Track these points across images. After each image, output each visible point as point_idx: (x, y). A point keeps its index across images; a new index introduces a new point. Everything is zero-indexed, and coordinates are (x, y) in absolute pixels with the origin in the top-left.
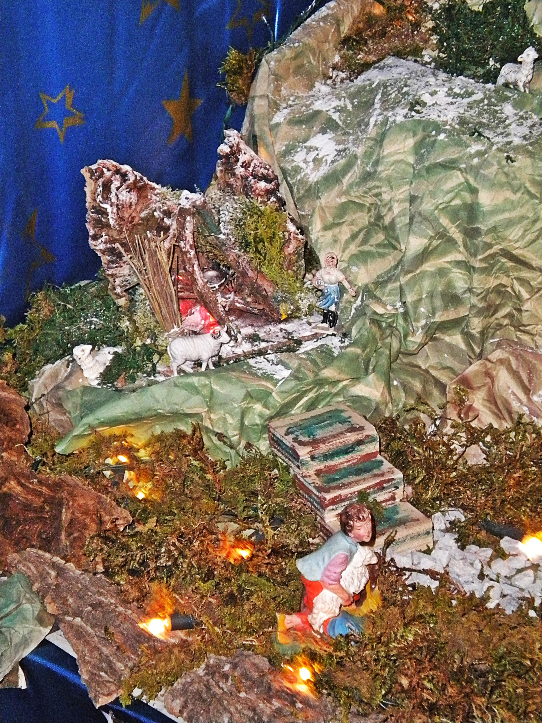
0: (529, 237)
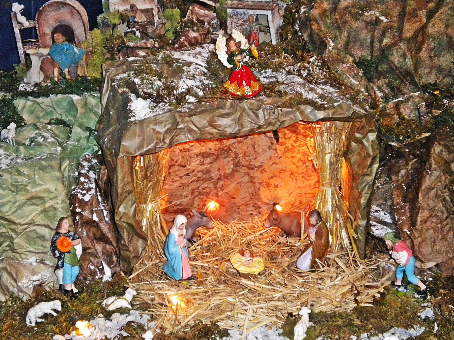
0: (13, 210)
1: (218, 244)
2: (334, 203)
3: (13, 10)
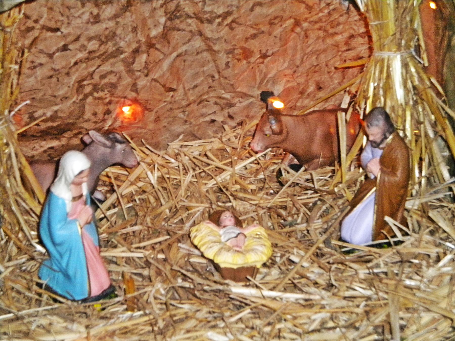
1: (152, 200)
2: (410, 85)
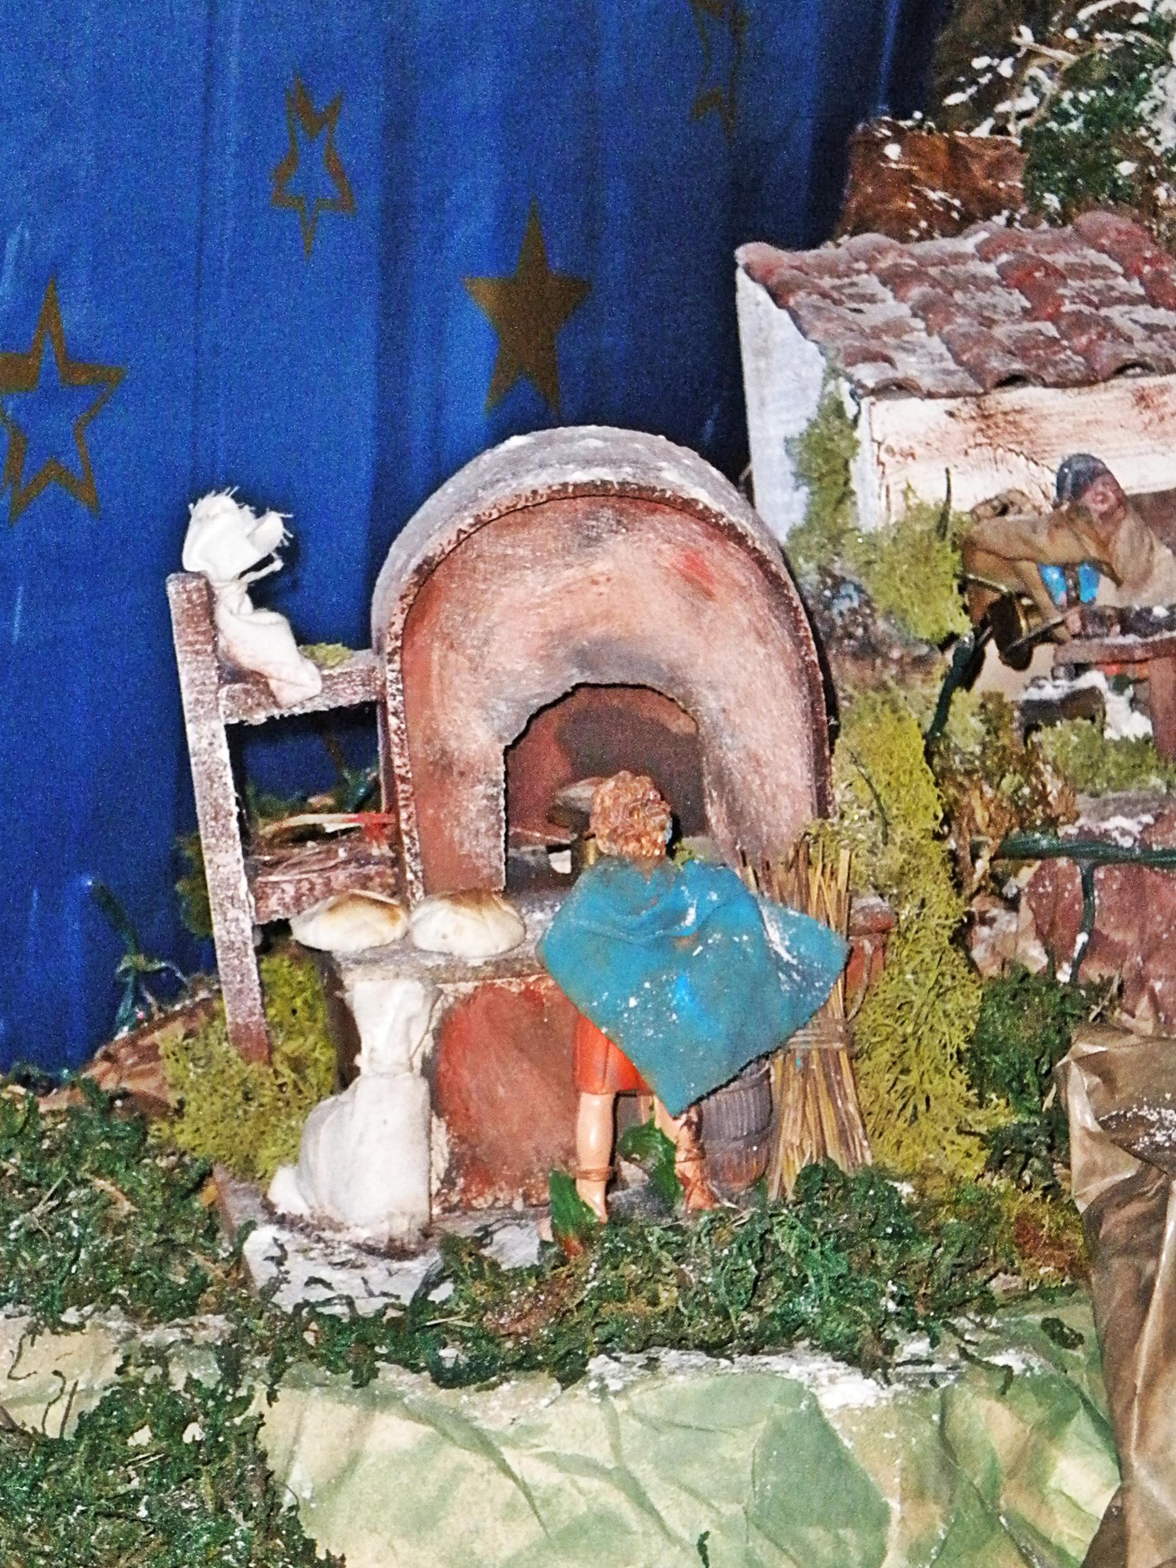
3: (192, 558)
